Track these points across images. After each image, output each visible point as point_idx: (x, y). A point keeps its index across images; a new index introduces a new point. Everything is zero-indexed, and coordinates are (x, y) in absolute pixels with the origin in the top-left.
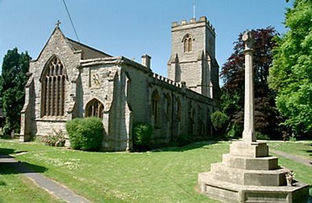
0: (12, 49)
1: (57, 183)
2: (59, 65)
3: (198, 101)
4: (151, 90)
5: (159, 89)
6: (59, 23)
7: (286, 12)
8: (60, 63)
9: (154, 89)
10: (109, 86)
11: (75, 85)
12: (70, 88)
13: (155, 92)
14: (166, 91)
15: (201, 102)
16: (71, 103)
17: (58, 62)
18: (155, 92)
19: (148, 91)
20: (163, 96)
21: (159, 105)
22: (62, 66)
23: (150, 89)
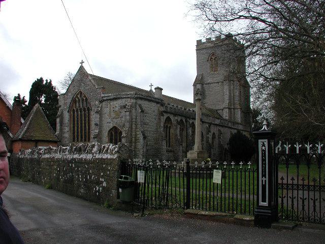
0: (39, 78)
1: (83, 156)
2: (84, 99)
3: (219, 125)
4: (163, 119)
5: (172, 117)
6: (82, 63)
7: (198, 12)
8: (85, 96)
9: (165, 117)
10: (125, 116)
11: (98, 116)
12: (94, 118)
13: (168, 119)
14: (179, 118)
15: (222, 126)
16: (95, 131)
17: (83, 96)
18: (168, 119)
19: (160, 119)
20: (175, 123)
21: (172, 131)
22: (86, 99)
23: (162, 117)
